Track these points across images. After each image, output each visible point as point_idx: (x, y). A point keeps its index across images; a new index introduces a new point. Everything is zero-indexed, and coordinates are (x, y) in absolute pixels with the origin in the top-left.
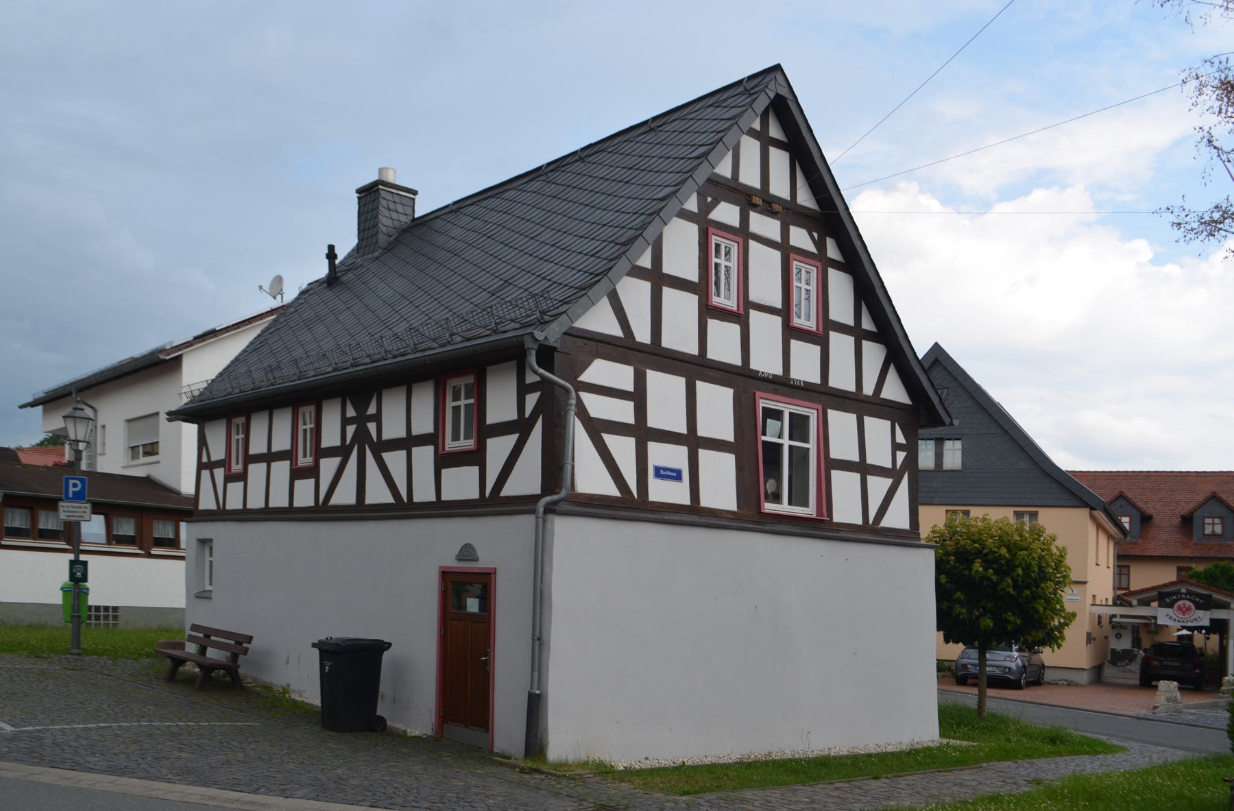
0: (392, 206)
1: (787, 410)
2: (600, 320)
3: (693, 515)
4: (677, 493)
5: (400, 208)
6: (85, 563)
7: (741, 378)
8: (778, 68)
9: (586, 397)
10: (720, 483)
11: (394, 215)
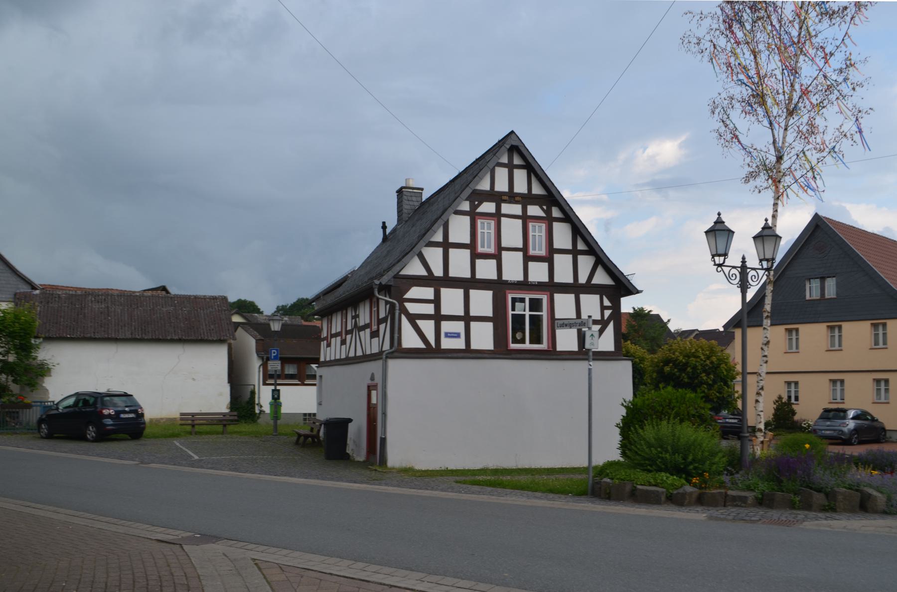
0: (410, 198)
1: (527, 297)
2: (415, 268)
3: (468, 353)
4: (460, 344)
5: (414, 199)
6: (279, 391)
7: (498, 287)
8: (512, 132)
9: (407, 305)
10: (483, 336)
11: (411, 203)
